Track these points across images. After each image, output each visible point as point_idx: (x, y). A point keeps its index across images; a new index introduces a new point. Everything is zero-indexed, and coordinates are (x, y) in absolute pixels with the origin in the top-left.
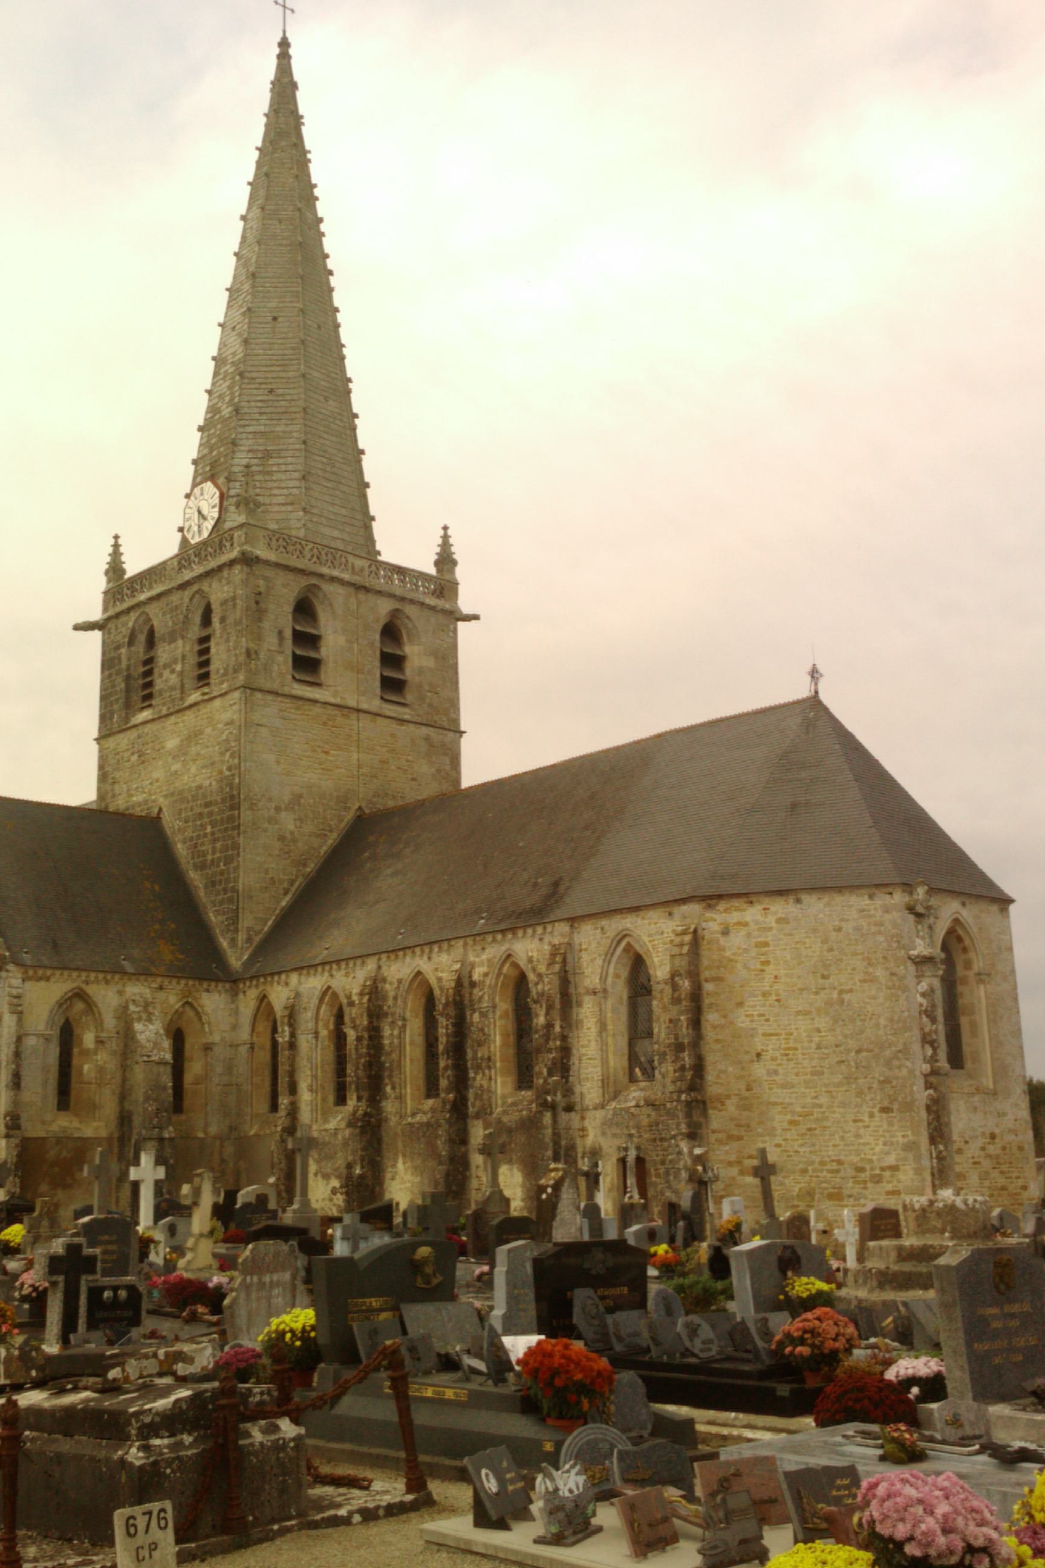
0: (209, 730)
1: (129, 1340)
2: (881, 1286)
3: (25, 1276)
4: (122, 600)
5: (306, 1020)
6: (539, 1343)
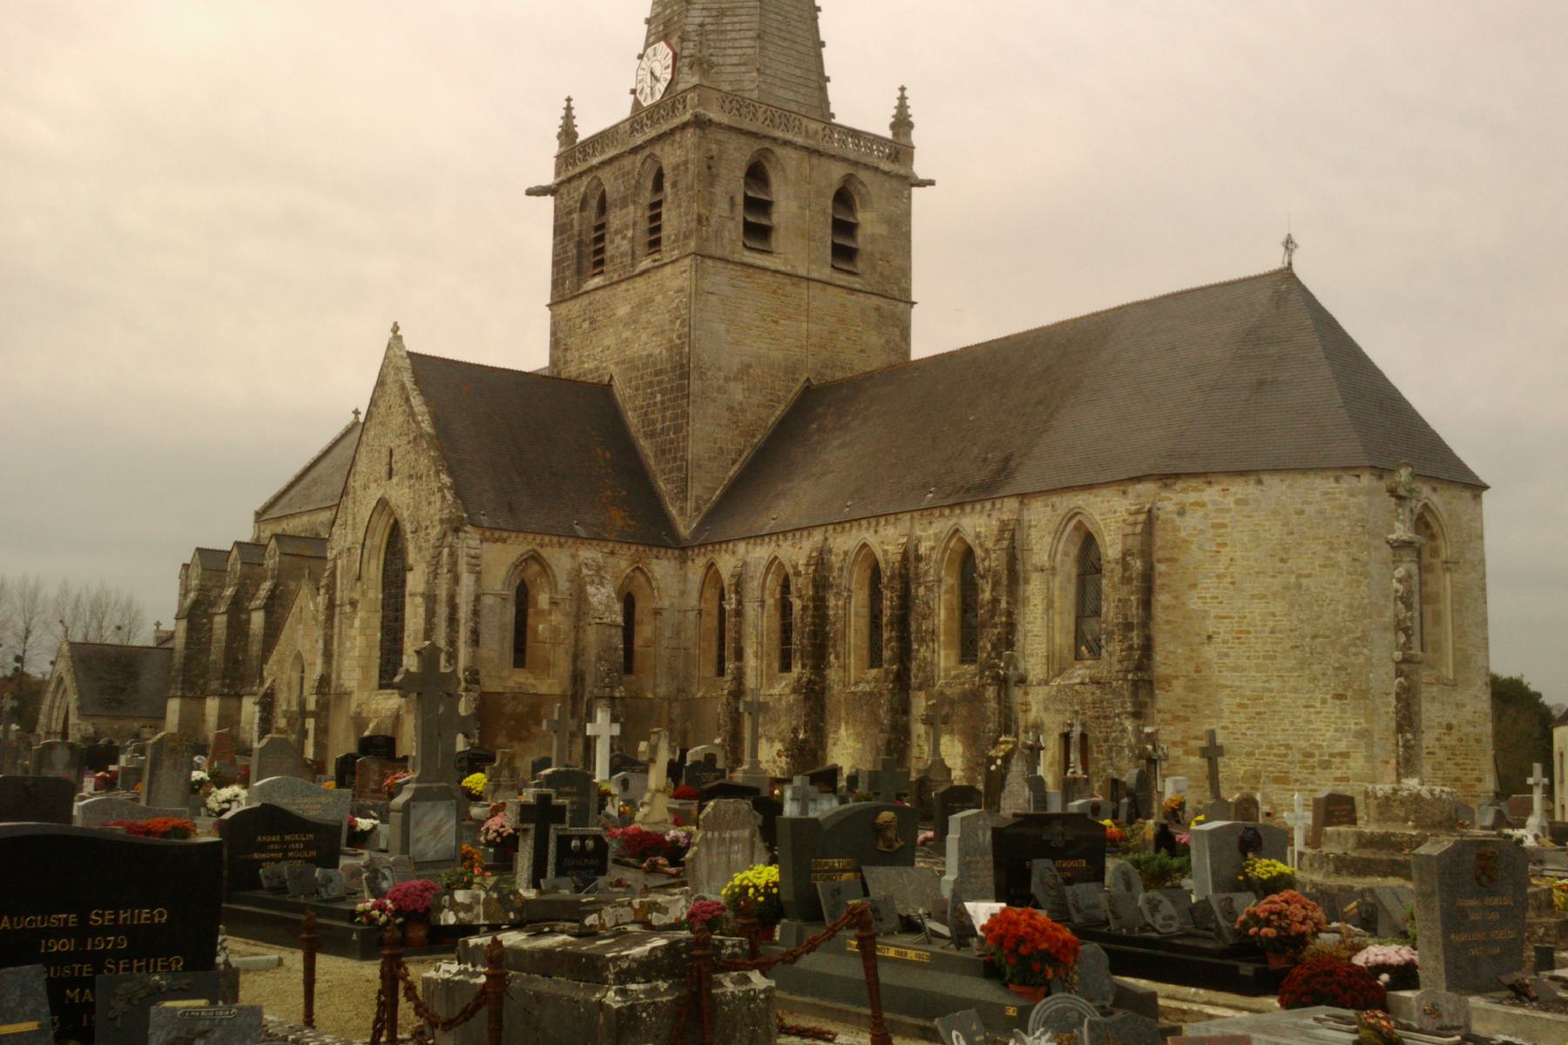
0: (659, 298)
1: (596, 887)
2: (1338, 871)
3: (490, 822)
4: (575, 165)
5: (753, 588)
6: (1003, 911)
